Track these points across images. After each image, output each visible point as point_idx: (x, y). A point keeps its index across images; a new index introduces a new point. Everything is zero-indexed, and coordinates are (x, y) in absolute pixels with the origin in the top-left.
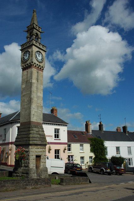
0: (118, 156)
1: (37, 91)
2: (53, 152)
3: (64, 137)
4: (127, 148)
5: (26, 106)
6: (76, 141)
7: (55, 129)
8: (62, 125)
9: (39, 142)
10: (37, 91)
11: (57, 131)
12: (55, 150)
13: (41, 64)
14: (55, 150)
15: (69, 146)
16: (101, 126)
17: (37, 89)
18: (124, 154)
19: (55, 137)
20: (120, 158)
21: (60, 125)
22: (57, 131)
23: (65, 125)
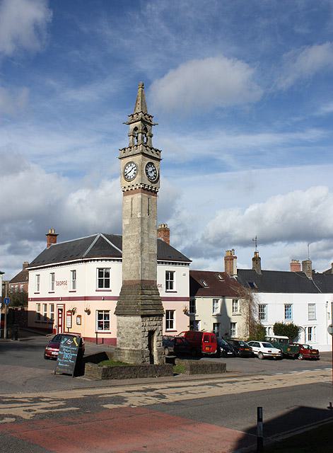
0: (287, 322)
1: (148, 231)
2: (94, 315)
3: (182, 286)
4: (284, 306)
5: (132, 255)
6: (206, 294)
7: (167, 273)
8: (179, 264)
9: (153, 312)
10: (148, 231)
11: (169, 275)
12: (166, 271)
13: (154, 185)
14: (166, 271)
15: (193, 303)
16: (256, 260)
17: (148, 227)
18: (298, 319)
19: (167, 288)
20: (292, 325)
21: (176, 264)
22: (169, 275)
23: (186, 264)
